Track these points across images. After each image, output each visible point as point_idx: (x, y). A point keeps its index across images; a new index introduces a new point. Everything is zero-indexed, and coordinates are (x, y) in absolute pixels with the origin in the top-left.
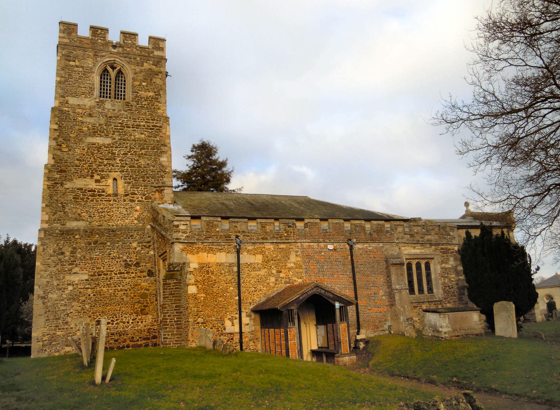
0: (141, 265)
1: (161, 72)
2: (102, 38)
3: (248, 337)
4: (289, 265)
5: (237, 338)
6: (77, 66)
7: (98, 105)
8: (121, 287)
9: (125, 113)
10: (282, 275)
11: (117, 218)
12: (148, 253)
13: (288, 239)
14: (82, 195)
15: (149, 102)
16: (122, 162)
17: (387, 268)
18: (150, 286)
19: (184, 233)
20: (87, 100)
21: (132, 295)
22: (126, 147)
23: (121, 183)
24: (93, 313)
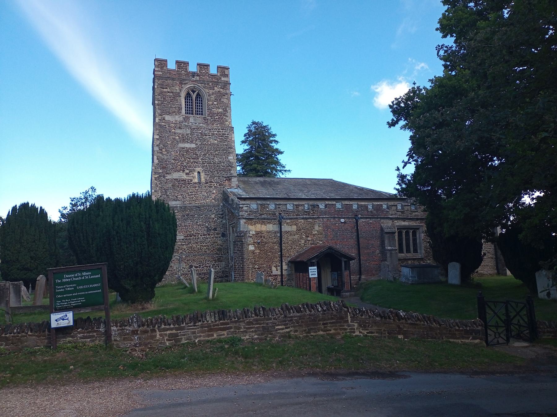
0: (217, 230)
1: (227, 94)
2: (185, 70)
3: (286, 278)
4: (314, 233)
5: (279, 278)
6: (168, 92)
7: (185, 120)
8: (205, 244)
9: (203, 125)
10: (309, 239)
11: (201, 198)
12: (222, 222)
13: (314, 216)
14: (177, 184)
15: (219, 116)
16: (203, 161)
17: (382, 235)
18: (223, 244)
19: (246, 212)
20: (177, 116)
21: (212, 249)
22: (205, 150)
23: (202, 175)
24: (188, 261)
